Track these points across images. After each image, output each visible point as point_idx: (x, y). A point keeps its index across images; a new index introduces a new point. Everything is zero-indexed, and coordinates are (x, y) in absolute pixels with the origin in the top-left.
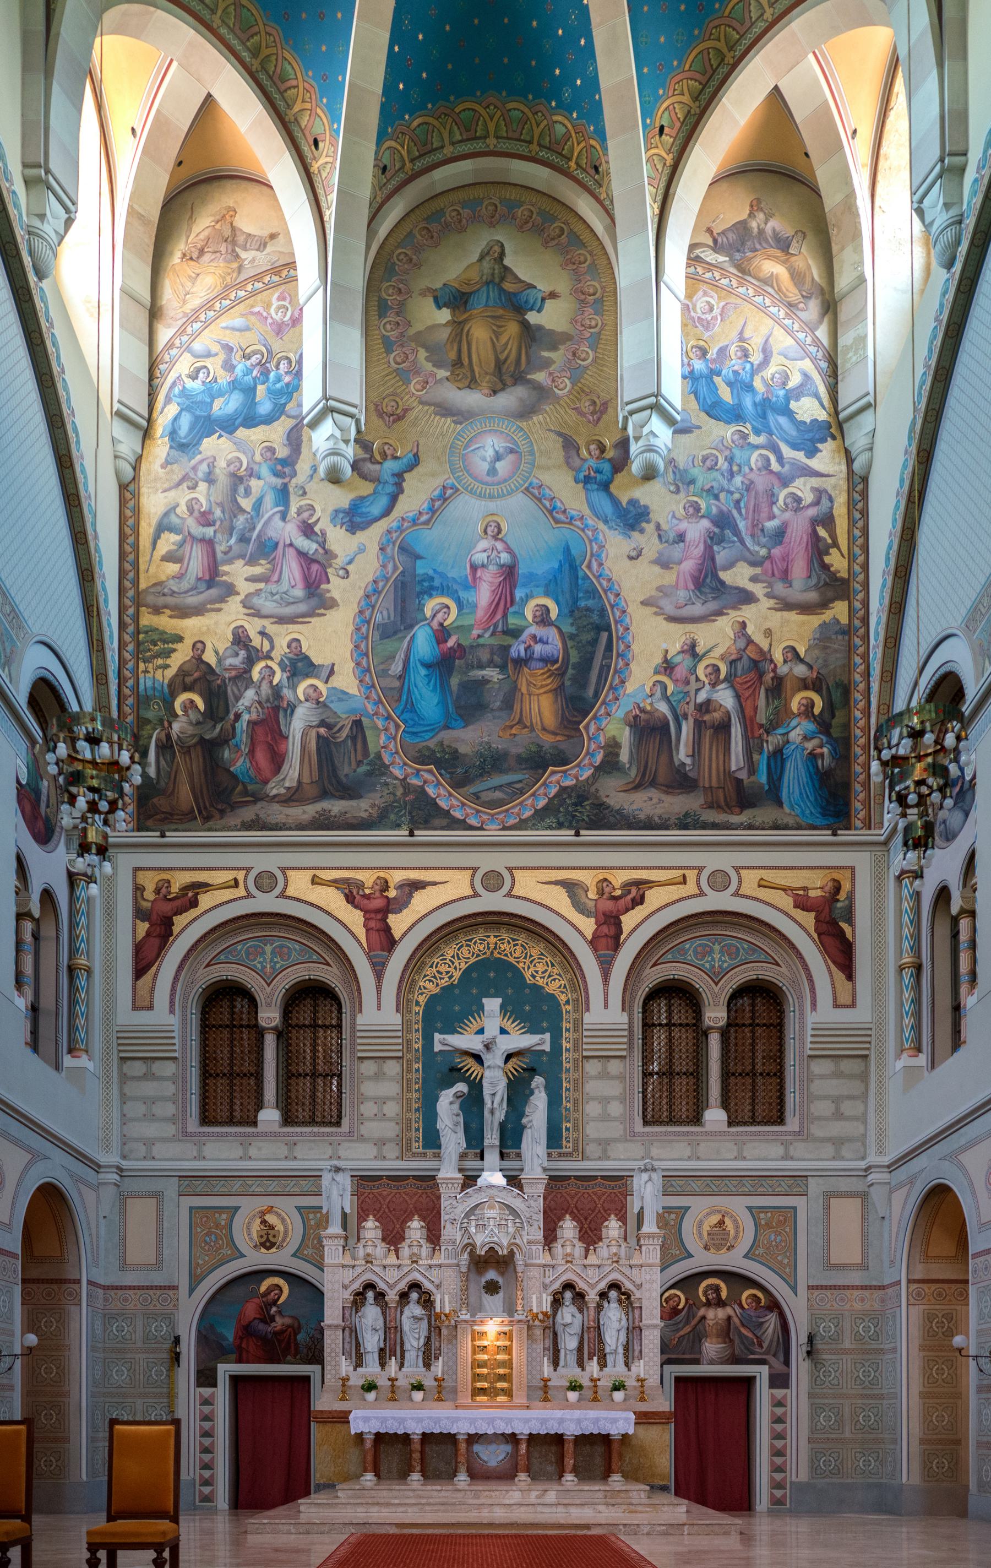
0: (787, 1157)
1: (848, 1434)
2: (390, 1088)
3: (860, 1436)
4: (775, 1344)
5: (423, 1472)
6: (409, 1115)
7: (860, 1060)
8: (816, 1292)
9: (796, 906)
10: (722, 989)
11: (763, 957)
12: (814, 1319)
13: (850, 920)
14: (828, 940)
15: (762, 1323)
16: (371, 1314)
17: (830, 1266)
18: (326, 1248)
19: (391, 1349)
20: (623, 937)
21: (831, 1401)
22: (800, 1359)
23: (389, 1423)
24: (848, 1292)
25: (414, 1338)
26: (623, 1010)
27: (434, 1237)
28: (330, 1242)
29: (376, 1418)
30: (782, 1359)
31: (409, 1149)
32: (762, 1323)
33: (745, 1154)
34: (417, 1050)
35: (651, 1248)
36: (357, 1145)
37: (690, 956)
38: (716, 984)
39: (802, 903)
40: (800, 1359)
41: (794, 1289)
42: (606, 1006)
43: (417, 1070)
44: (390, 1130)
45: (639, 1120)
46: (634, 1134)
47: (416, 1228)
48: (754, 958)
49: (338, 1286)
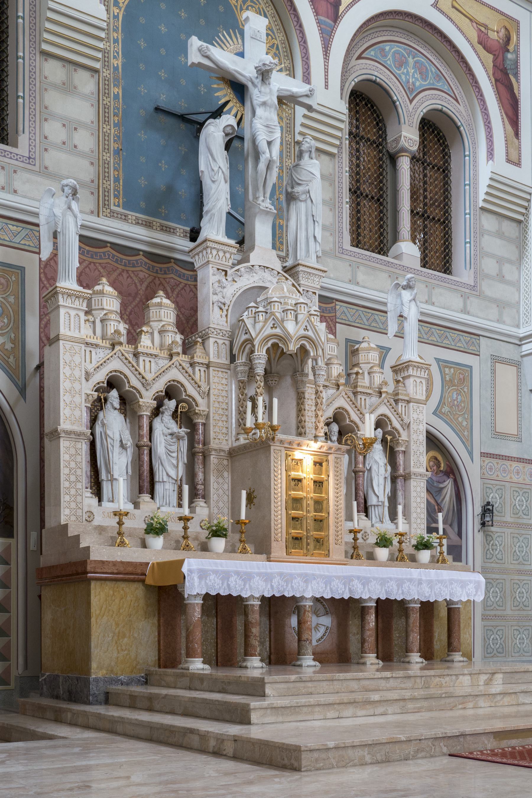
0: (465, 311)
1: (509, 612)
2: (82, 110)
3: (517, 613)
4: (451, 513)
5: (428, 654)
6: (106, 156)
7: (514, 225)
8: (487, 460)
9: (480, 43)
10: (416, 109)
11: (446, 88)
12: (485, 489)
13: (517, 75)
14: (502, 88)
15: (442, 489)
16: (114, 423)
17: (498, 435)
18: (62, 311)
19: (145, 482)
20: (342, 8)
21: (497, 576)
22: (476, 531)
23: (275, 582)
24: (508, 463)
25: (170, 466)
26: (341, 99)
27: (189, 324)
28: (68, 302)
29: (216, 572)
30: (456, 529)
31: (106, 205)
32: (442, 489)
33: (434, 300)
34: (116, 69)
35: (418, 380)
36: (39, 179)
37: (390, 62)
38: (411, 101)
39: (483, 42)
40: (476, 531)
41: (471, 454)
42: (327, 87)
43: (116, 97)
44: (83, 170)
45: (347, 238)
46: (343, 251)
47: (163, 311)
48: (439, 85)
49: (79, 373)
